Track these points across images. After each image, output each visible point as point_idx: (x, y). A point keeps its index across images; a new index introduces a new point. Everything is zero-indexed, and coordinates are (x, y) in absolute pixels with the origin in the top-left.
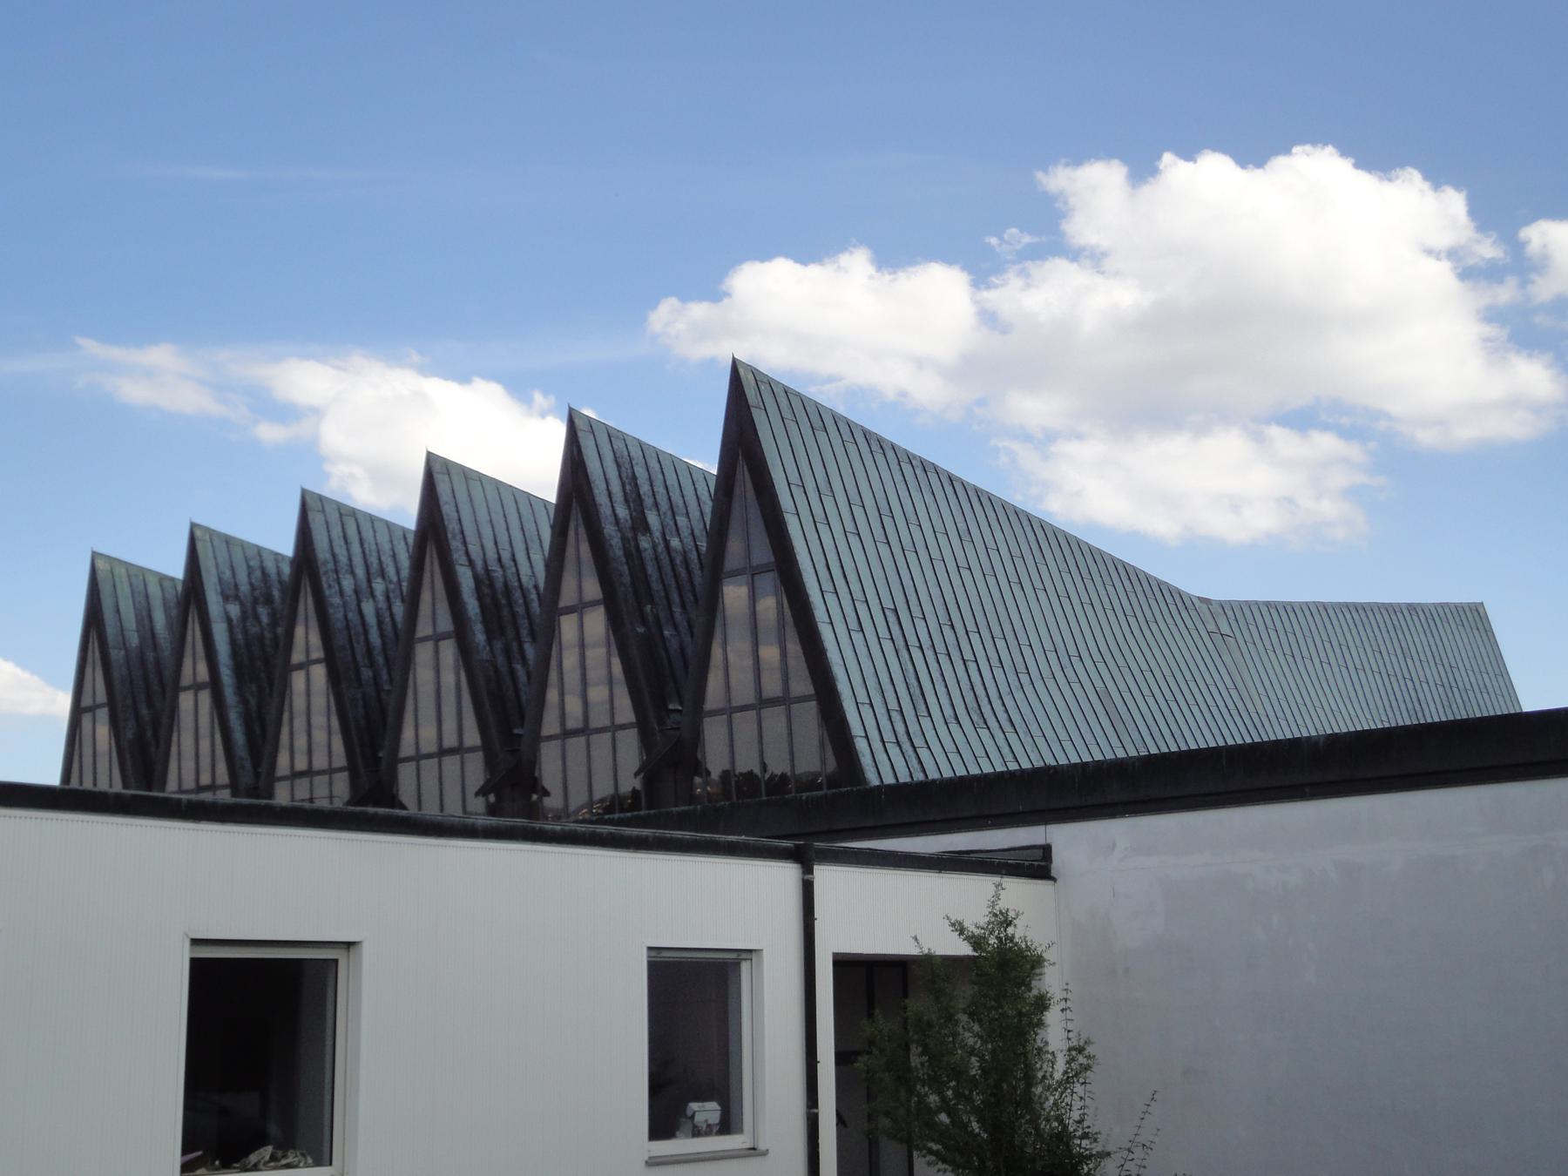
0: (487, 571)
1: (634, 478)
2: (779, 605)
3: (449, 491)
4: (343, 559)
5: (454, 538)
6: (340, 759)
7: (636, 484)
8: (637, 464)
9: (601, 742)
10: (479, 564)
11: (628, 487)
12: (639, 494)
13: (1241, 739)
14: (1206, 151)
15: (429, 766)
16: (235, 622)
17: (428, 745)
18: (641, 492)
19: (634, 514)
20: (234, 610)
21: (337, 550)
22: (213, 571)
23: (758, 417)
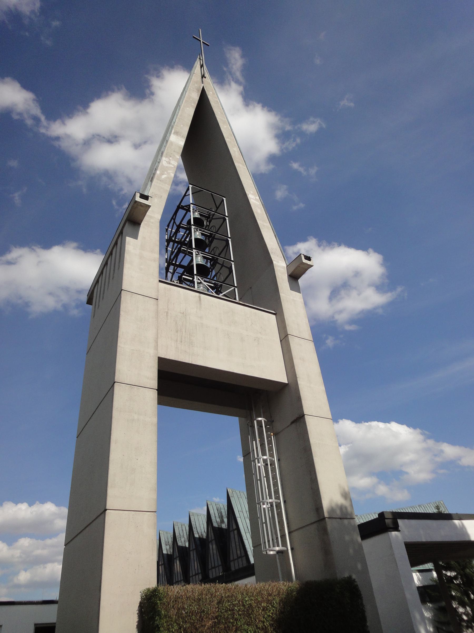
0: (202, 535)
1: (221, 512)
2: (216, 546)
3: (193, 519)
4: (182, 534)
5: (194, 529)
6: (220, 563)
7: (222, 514)
8: (222, 509)
9: (217, 569)
10: (200, 534)
11: (220, 514)
12: (222, 515)
13: (415, 511)
14: (49, 502)
15: (236, 561)
16: (168, 550)
17: (194, 573)
18: (223, 515)
19: (221, 520)
20: (168, 547)
21: (180, 533)
22: (164, 539)
23: (231, 498)
